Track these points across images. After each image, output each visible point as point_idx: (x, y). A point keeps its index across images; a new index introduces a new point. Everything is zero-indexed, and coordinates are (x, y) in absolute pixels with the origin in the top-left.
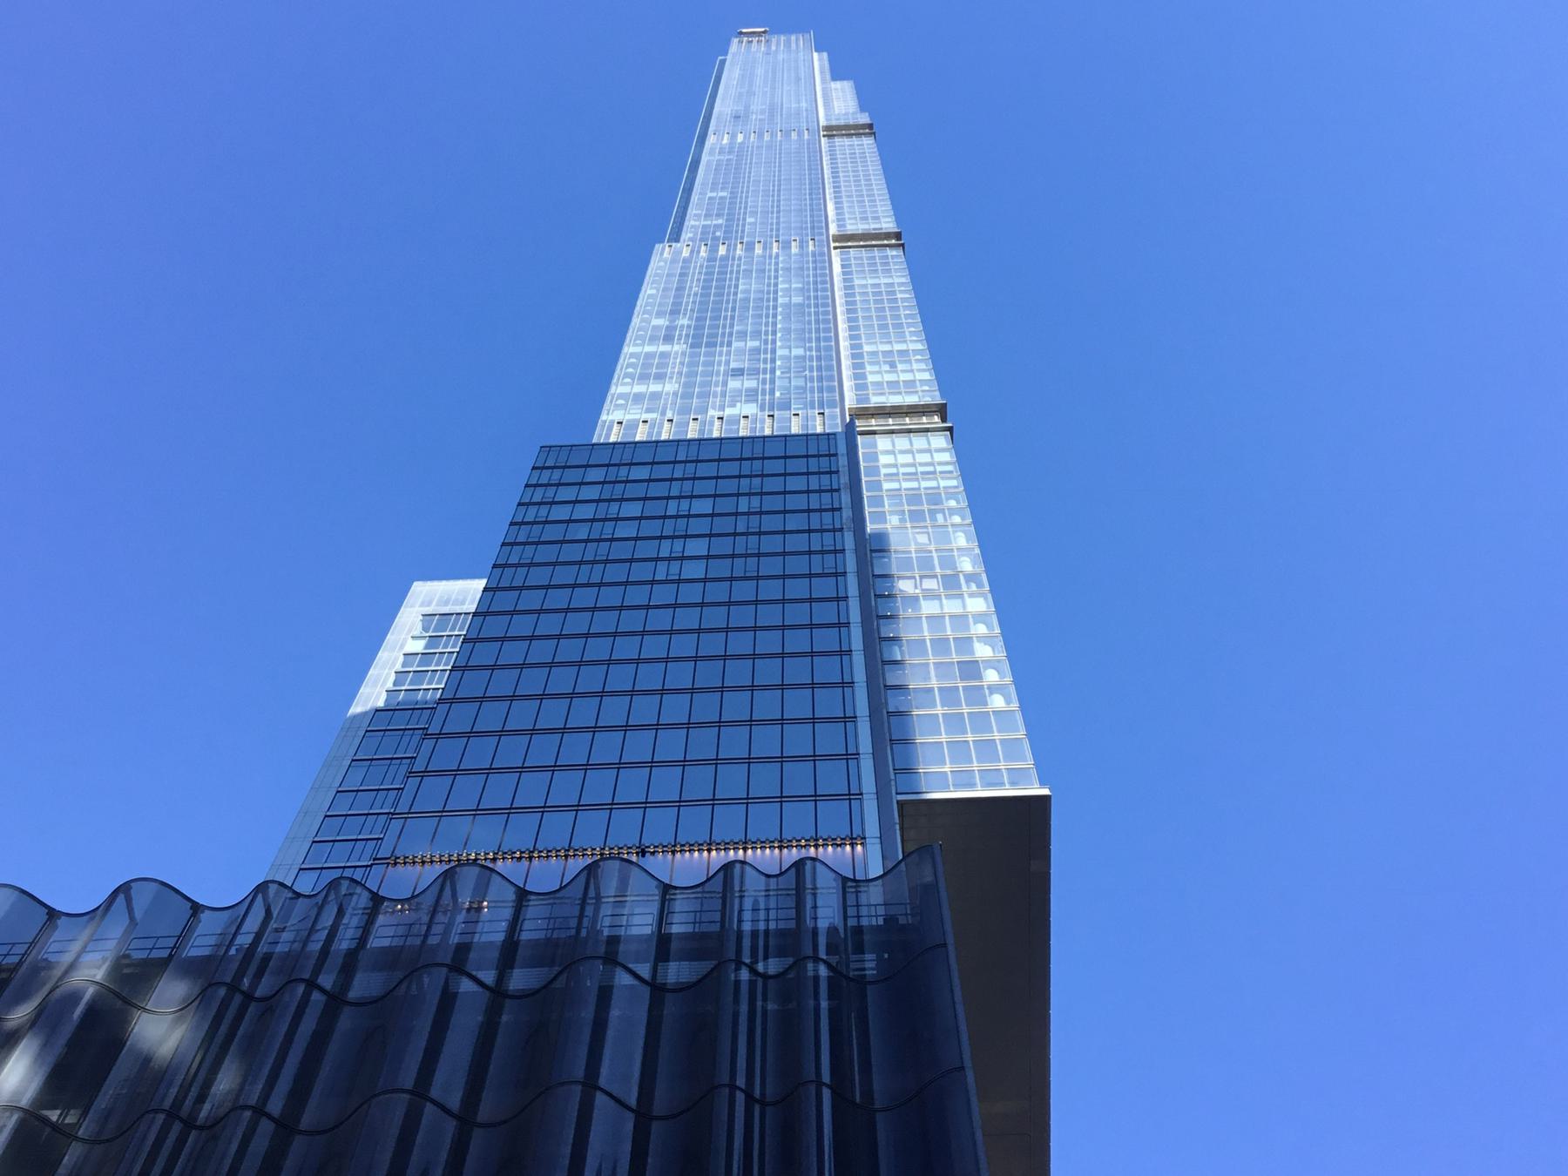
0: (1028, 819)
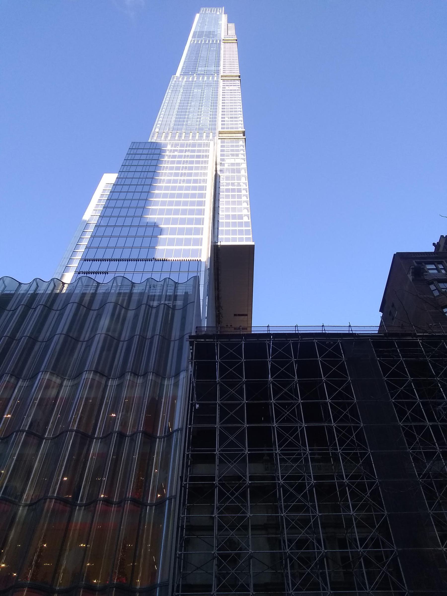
0: (248, 251)
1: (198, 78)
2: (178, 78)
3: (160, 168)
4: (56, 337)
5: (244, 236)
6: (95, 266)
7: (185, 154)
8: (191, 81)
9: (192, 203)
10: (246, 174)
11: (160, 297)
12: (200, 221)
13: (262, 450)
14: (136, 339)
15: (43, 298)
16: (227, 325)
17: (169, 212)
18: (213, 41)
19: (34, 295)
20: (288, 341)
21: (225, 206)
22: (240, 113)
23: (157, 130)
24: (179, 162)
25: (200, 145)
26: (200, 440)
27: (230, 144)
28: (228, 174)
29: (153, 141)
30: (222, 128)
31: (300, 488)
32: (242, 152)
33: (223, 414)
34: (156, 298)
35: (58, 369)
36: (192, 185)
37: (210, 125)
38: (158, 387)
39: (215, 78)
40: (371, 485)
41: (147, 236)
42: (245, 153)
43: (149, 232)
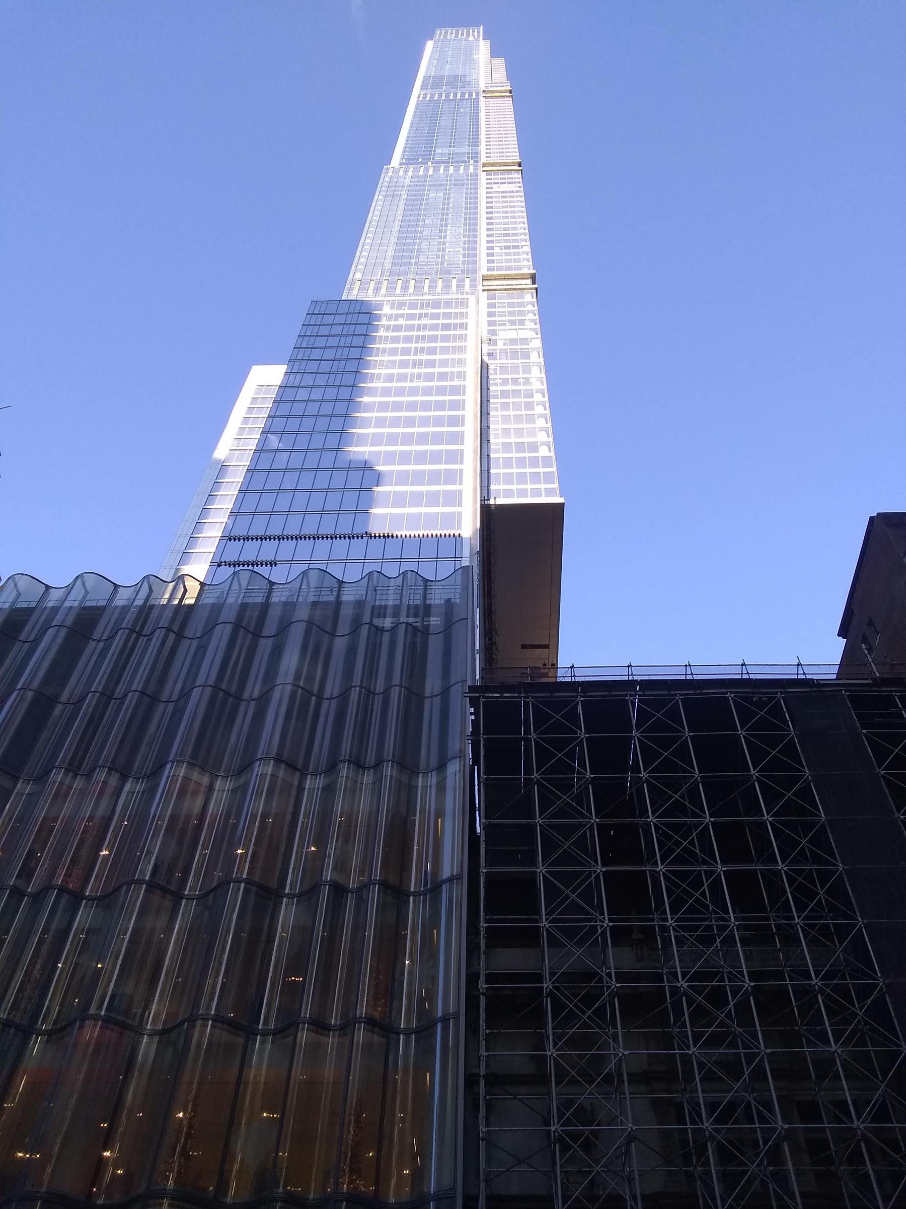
1: (436, 170)
2: (396, 171)
3: (370, 352)
4: (196, 693)
5: (543, 486)
6: (250, 551)
7: (420, 322)
8: (421, 177)
9: (439, 422)
10: (542, 360)
11: (397, 608)
12: (456, 457)
13: (629, 920)
14: (354, 695)
15: (128, 616)
16: (545, 665)
17: (393, 439)
18: (463, 95)
19: (147, 610)
20: (673, 695)
21: (500, 426)
22: (523, 237)
23: (358, 276)
24: (408, 339)
25: (448, 304)
26: (502, 899)
27: (506, 301)
28: (504, 361)
29: (351, 297)
30: (488, 270)
31: (718, 998)
32: (531, 316)
33: (549, 846)
34: (389, 611)
35: (203, 757)
36: (435, 384)
37: (463, 263)
38: (405, 794)
39: (471, 168)
40: (864, 992)
41: (335, 490)
42: (537, 317)
43: (355, 479)
